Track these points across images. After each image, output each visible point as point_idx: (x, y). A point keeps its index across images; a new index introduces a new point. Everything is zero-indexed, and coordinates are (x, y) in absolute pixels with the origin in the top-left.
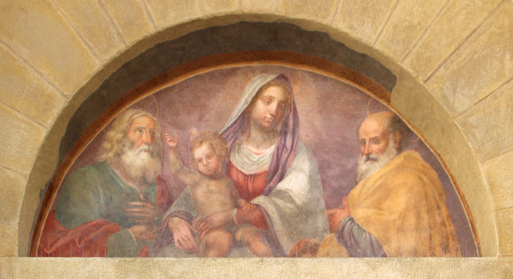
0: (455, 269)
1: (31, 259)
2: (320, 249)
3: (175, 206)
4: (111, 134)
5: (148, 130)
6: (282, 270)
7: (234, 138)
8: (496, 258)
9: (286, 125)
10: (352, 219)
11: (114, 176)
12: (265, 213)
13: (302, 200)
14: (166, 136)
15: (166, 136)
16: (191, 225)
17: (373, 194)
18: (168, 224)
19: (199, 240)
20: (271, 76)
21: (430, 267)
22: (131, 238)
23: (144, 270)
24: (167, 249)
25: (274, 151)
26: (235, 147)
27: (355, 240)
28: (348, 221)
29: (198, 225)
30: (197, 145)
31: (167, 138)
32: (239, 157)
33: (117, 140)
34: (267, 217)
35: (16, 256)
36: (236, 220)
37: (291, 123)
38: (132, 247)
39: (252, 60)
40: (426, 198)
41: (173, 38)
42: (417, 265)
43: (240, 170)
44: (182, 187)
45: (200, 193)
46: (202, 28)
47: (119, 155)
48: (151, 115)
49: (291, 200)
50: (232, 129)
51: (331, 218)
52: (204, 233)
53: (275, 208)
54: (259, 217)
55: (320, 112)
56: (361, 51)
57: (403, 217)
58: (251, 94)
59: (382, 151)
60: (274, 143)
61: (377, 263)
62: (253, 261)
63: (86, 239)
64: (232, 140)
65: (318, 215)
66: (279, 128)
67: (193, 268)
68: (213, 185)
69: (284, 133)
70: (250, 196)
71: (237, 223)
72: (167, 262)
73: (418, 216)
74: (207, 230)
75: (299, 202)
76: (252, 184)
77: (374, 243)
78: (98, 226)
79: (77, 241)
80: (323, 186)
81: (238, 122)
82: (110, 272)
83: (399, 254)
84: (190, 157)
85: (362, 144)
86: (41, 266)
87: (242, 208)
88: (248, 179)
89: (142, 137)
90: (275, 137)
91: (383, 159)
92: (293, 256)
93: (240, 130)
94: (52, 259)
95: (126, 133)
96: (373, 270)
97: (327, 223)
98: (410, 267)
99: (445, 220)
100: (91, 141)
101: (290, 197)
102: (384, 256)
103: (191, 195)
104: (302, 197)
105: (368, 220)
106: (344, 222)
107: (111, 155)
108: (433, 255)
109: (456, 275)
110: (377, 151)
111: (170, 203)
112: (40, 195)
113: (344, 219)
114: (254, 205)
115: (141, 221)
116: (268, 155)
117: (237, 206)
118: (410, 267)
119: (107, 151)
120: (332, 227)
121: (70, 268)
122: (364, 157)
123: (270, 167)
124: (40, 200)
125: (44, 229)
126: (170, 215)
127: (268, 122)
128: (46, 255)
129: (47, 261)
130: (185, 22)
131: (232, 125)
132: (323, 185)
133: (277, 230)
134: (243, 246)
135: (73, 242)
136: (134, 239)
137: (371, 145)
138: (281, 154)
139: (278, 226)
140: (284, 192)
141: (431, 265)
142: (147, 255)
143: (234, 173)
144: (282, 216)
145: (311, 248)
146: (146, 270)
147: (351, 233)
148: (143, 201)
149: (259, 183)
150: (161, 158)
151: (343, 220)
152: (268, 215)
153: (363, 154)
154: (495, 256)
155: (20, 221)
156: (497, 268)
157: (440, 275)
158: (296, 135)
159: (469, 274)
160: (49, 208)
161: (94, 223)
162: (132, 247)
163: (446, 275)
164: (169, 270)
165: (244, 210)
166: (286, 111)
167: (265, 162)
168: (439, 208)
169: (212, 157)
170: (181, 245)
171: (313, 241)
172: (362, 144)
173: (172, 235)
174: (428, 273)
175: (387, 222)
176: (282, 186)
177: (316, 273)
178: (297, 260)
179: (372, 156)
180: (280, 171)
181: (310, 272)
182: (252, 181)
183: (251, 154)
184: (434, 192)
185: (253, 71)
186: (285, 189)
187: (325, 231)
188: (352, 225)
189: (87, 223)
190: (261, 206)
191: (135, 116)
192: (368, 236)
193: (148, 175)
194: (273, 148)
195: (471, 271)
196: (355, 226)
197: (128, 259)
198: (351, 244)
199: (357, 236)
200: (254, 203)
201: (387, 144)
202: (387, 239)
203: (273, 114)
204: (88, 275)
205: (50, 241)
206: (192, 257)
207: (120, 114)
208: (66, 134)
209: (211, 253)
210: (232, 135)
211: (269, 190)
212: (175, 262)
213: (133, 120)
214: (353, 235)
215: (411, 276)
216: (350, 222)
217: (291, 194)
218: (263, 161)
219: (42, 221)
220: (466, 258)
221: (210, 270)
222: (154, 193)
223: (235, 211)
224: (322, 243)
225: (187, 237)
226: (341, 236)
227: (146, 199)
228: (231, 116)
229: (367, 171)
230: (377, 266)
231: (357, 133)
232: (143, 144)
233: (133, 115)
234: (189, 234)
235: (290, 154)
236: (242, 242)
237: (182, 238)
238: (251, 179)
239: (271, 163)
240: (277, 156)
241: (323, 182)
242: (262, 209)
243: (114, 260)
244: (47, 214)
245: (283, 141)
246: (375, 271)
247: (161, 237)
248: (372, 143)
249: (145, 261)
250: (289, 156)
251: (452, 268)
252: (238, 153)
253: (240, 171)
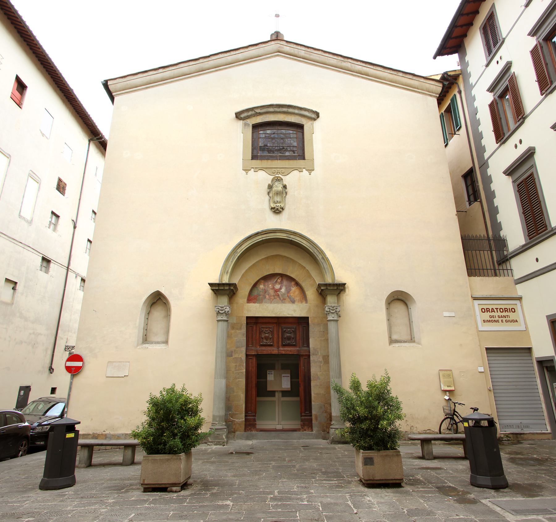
44: (268, 290)
45: (270, 291)
49: (282, 292)
51: (288, 295)
57: (297, 295)
68: (272, 290)
69: (282, 284)
70: (277, 292)
78: (256, 296)
90: (185, 401)
105: (292, 296)
111: (266, 293)
117: (275, 293)
139: (280, 296)
144: (281, 295)
149: (278, 290)
171: (285, 298)
176: (281, 290)
227: (263, 292)
240: (281, 287)
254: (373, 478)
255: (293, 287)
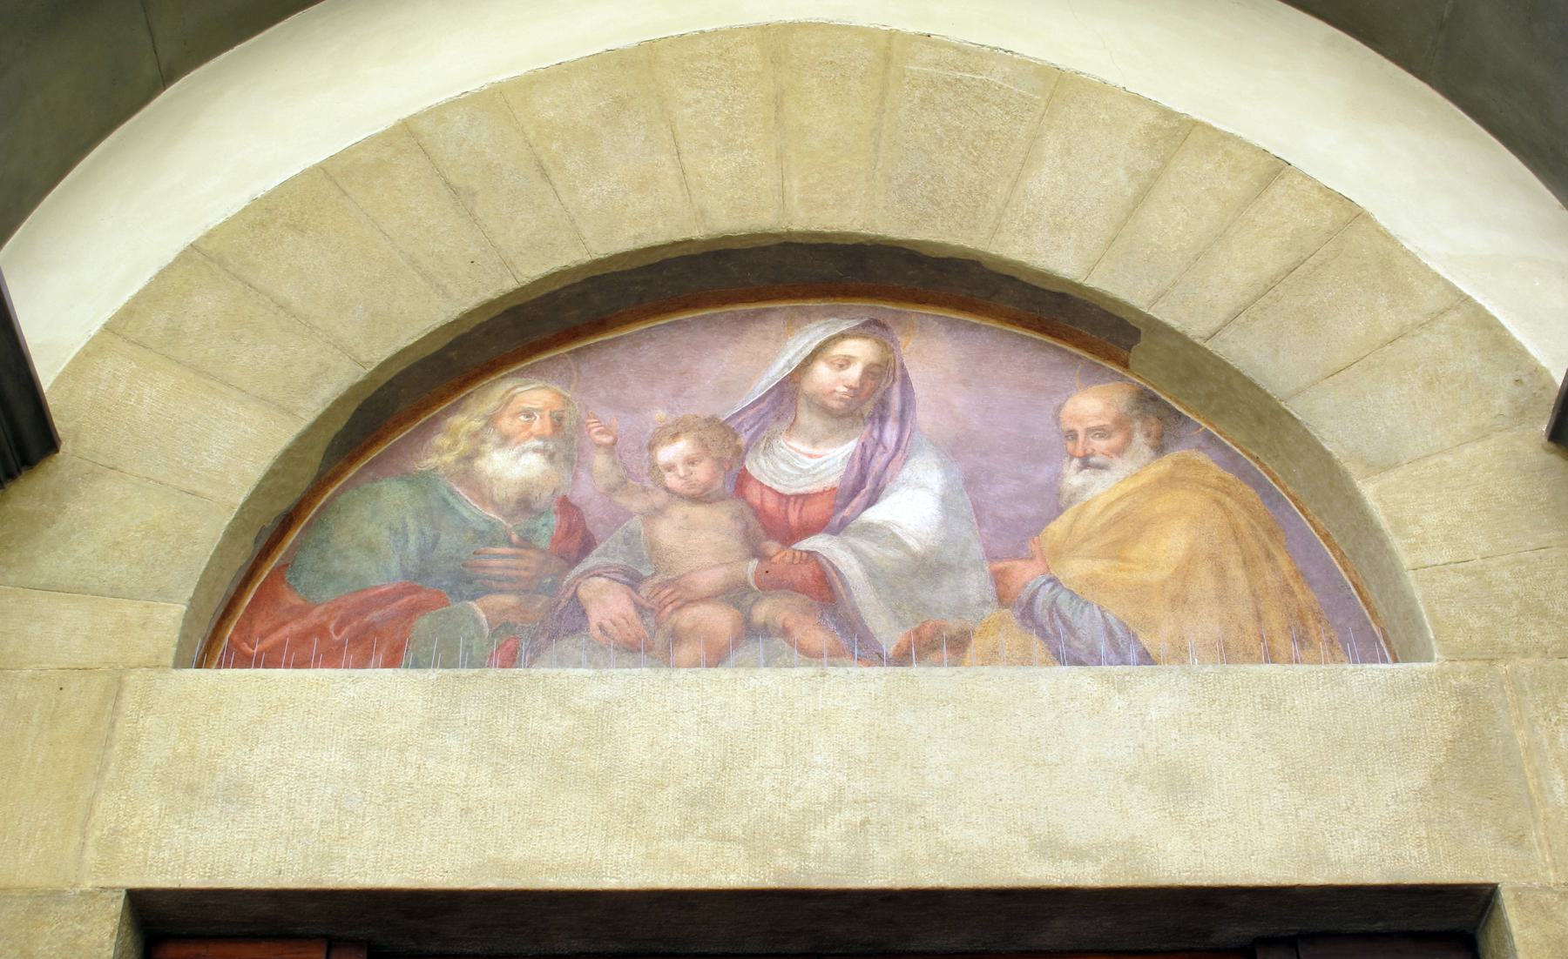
0: (1332, 689)
1: (202, 672)
2: (974, 641)
3: (598, 556)
4: (457, 420)
5: (547, 413)
6: (875, 695)
7: (757, 427)
8: (1433, 665)
9: (883, 404)
10: (1053, 580)
11: (450, 499)
12: (830, 568)
13: (925, 542)
14: (589, 423)
15: (589, 423)
16: (638, 593)
17: (1104, 530)
18: (576, 591)
19: (657, 623)
20: (847, 322)
21: (1267, 684)
22: (476, 620)
23: (504, 696)
24: (567, 645)
25: (855, 450)
26: (758, 444)
27: (1064, 623)
28: (1044, 584)
29: (656, 592)
30: (665, 439)
31: (593, 428)
32: (766, 463)
33: (469, 432)
34: (834, 575)
35: (167, 667)
36: (756, 582)
37: (895, 401)
38: (477, 638)
39: (805, 296)
40: (1237, 536)
41: (628, 268)
42: (1233, 681)
43: (769, 485)
46: (693, 252)
47: (469, 458)
48: (558, 388)
49: (899, 544)
50: (751, 412)
52: (669, 608)
53: (856, 558)
54: (813, 577)
55: (966, 383)
56: (1057, 289)
57: (1184, 571)
58: (801, 351)
59: (1119, 451)
60: (855, 437)
61: (1127, 678)
62: (798, 675)
63: (355, 624)
64: (752, 431)
65: (967, 573)
66: (868, 408)
67: (637, 692)
69: (880, 416)
70: (790, 536)
71: (756, 588)
72: (568, 677)
73: (1221, 573)
74: (679, 603)
75: (916, 547)
76: (797, 511)
77: (1116, 628)
79: (332, 626)
80: (977, 516)
81: (767, 400)
82: (412, 701)
83: (1179, 654)
84: (645, 462)
85: (1070, 438)
86: (228, 687)
87: (771, 558)
88: (787, 503)
89: (530, 426)
91: (1122, 468)
92: (902, 658)
93: (772, 414)
94: (262, 672)
95: (491, 420)
96: (1120, 693)
97: (991, 588)
98: (1215, 685)
99: (1291, 582)
100: (404, 434)
101: (894, 535)
102: (1146, 658)
103: (642, 533)
104: (923, 537)
106: (1033, 586)
107: (449, 458)
108: (1271, 657)
109: (1337, 701)
110: (1107, 452)
111: (587, 546)
112: (256, 541)
113: (1032, 579)
114: (801, 552)
115: (506, 585)
116: (840, 459)
117: (757, 553)
118: (1215, 685)
119: (440, 451)
120: (1004, 596)
121: (305, 693)
122: (1076, 462)
123: (843, 479)
124: (255, 547)
125: (252, 600)
126: (584, 573)
127: (841, 399)
128: (244, 661)
129: (246, 677)
130: (657, 244)
131: (753, 405)
132: (976, 513)
133: (860, 602)
134: (769, 637)
135: (322, 630)
136: (484, 622)
137: (1091, 440)
138: (872, 456)
140: (879, 526)
141: (1270, 681)
142: (511, 660)
143: (754, 494)
145: (952, 638)
146: (510, 695)
147: (1054, 609)
148: (518, 546)
149: (815, 511)
150: (572, 464)
151: (1032, 582)
152: (838, 572)
153: (1072, 457)
154: (1430, 660)
155: (194, 594)
156: (1440, 685)
157: (1297, 702)
158: (909, 425)
159: (1372, 700)
160: (272, 561)
161: (383, 590)
162: (477, 638)
163: (1313, 702)
164: (572, 694)
165: (775, 563)
166: (884, 380)
167: (831, 471)
168: (1269, 556)
169: (701, 462)
170: (606, 634)
172: (1070, 438)
173: (584, 613)
174: (1262, 697)
175: (1145, 586)
176: (873, 515)
177: (967, 699)
178: (915, 670)
179: (1093, 460)
180: (868, 487)
181: (952, 697)
182: (798, 506)
183: (796, 457)
184: (1253, 527)
185: (809, 316)
186: (881, 522)
187: (985, 603)
188: (1054, 592)
189: (365, 590)
190: (822, 556)
191: (519, 389)
192: (1098, 614)
193: (538, 495)
194: (851, 446)
195: (1375, 693)
196: (1064, 593)
197: (464, 672)
198: (1054, 629)
199: (1069, 614)
200: (803, 549)
201: (1129, 439)
202: (1148, 619)
203: (854, 385)
204: (350, 706)
205: (260, 627)
206: (637, 665)
207: (484, 385)
208: (346, 426)
209: (685, 652)
210: (751, 422)
211: (841, 522)
212: (590, 678)
213: (514, 396)
214: (1058, 611)
215: (1221, 705)
216: (1049, 586)
217: (897, 531)
218: (826, 470)
219: (249, 588)
220: (1359, 666)
221: (681, 695)
222: (548, 528)
223: (753, 564)
224: (978, 628)
225: (624, 618)
226: (1027, 614)
228: (752, 387)
229: (1084, 488)
230: (1128, 685)
231: (1057, 418)
232: (533, 438)
233: (515, 387)
234: (631, 611)
235: (894, 456)
236: (769, 626)
237: (611, 620)
238: (795, 503)
239: (847, 472)
241: (978, 509)
242: (825, 562)
243: (426, 676)
244: (267, 572)
245: (876, 434)
246: (1124, 694)
247: (555, 618)
248: (1092, 437)
249: (510, 675)
250: (890, 461)
251: (1325, 686)
252: (765, 454)
253: (770, 489)
254: (116, 917)
255: (1086, 463)
